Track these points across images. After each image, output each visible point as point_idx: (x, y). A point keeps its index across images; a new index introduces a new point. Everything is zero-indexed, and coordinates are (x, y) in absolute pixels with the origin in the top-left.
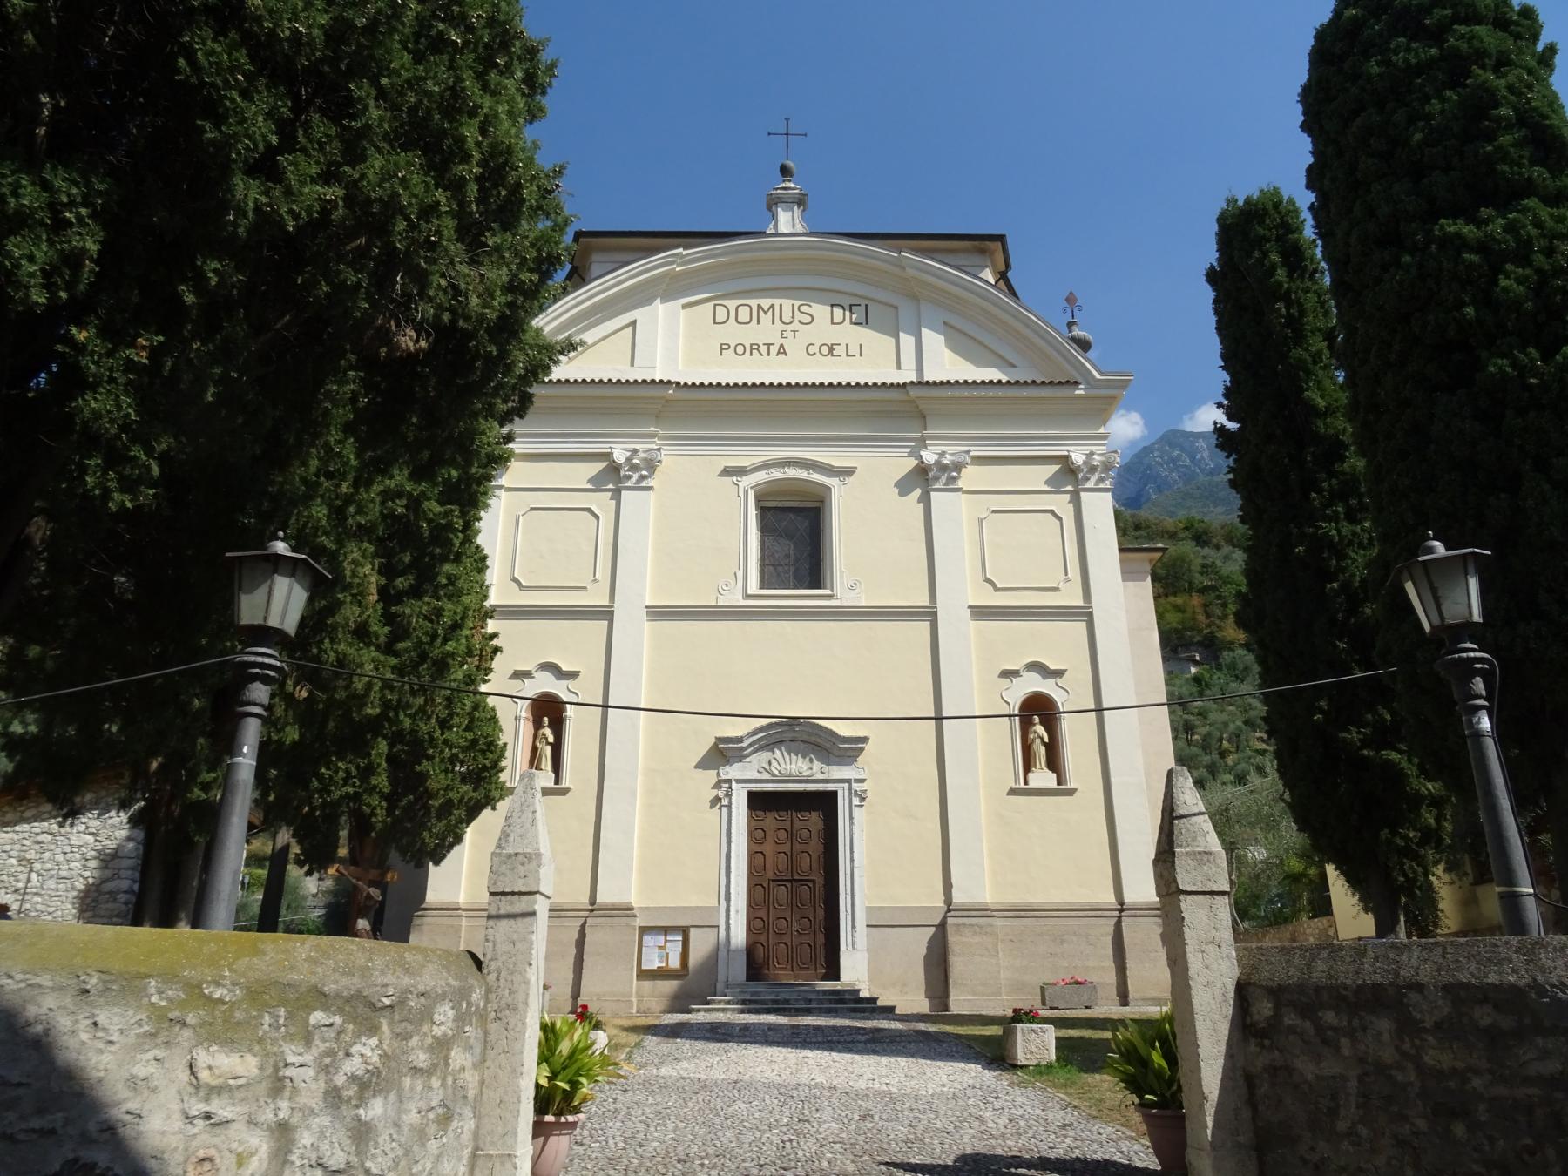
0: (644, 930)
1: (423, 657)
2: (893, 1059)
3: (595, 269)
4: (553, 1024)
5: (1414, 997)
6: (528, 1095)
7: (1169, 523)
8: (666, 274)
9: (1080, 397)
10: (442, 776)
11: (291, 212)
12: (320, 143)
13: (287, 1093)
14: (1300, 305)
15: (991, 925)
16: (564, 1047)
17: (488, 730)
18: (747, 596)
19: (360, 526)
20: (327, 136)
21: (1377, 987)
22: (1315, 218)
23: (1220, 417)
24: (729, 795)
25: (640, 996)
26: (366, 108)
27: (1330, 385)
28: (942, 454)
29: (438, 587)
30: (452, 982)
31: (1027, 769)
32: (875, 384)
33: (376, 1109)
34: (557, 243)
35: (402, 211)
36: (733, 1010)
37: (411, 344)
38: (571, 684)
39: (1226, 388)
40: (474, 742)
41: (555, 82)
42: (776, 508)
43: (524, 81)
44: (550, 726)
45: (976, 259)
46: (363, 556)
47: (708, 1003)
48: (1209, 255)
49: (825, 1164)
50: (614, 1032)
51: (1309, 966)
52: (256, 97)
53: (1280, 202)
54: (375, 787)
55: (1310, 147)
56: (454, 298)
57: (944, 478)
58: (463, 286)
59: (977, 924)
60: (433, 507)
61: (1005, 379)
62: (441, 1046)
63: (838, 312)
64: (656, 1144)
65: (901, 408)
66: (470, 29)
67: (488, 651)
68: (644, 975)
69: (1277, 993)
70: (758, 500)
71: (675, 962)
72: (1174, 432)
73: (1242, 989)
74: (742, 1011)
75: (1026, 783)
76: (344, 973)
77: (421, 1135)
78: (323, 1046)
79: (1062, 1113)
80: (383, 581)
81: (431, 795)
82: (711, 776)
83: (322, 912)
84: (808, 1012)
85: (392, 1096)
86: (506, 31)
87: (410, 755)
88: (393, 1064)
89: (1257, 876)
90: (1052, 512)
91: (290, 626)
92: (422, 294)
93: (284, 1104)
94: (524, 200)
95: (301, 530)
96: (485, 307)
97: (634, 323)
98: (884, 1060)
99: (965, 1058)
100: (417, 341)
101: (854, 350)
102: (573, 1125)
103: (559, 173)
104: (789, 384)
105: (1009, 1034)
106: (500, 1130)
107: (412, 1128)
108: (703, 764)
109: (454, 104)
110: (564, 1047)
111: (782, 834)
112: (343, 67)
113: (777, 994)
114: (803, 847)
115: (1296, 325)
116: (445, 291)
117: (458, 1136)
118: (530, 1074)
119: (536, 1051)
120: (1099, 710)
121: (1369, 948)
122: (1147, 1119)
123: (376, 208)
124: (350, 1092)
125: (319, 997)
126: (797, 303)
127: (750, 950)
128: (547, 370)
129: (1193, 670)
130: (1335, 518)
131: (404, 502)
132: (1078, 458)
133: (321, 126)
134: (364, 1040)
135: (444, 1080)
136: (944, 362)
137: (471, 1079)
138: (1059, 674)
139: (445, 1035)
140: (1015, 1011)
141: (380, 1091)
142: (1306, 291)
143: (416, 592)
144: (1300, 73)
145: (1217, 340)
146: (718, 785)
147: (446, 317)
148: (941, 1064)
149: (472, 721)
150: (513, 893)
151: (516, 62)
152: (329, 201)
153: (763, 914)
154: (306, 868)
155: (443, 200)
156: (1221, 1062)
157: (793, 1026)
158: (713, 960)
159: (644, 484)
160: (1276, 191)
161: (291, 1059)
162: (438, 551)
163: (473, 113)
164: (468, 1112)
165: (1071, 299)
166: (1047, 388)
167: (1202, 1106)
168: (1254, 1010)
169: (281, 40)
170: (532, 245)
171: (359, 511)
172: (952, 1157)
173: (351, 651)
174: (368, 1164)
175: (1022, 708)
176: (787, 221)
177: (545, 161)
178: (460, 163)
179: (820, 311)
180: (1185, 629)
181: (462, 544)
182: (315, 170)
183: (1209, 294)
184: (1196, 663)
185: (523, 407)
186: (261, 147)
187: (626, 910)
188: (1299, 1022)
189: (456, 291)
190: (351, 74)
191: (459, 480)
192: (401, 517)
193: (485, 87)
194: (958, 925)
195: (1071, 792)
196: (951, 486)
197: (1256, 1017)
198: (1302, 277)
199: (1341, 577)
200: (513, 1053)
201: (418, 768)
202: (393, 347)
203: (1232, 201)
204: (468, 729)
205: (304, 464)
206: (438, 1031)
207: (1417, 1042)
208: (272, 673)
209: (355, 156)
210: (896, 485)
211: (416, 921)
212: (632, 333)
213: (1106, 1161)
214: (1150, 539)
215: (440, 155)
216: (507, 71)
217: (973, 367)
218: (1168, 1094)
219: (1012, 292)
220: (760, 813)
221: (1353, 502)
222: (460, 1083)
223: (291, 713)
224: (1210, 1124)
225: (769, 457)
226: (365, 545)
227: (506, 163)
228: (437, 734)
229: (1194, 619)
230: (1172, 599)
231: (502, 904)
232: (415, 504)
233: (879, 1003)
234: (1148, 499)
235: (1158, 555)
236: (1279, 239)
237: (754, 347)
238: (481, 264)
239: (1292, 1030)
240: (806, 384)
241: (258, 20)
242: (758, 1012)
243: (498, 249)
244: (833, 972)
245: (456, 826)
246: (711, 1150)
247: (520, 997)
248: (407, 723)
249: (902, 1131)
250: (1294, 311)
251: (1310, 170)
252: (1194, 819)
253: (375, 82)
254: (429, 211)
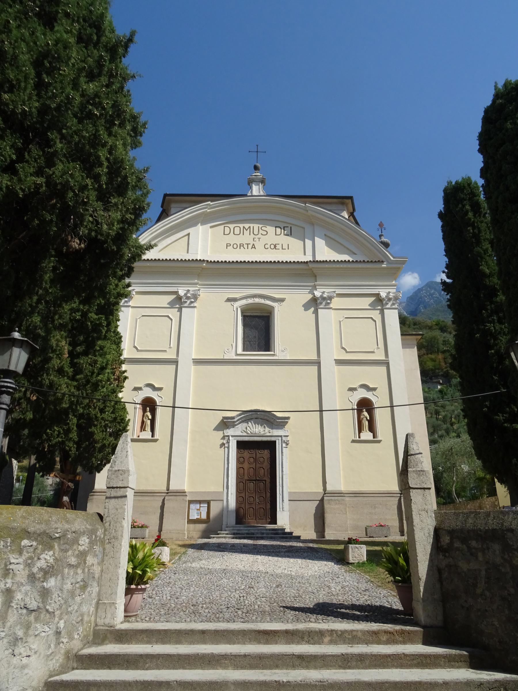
0: (190, 502)
1: (88, 382)
2: (295, 560)
3: (173, 210)
4: (136, 545)
5: (509, 534)
6: (123, 577)
7: (429, 322)
8: (203, 213)
9: (384, 268)
10: (101, 434)
11: (21, 189)
12: (35, 159)
13: (11, 576)
14: (479, 228)
15: (343, 500)
16: (140, 555)
17: (121, 413)
18: (237, 355)
19: (60, 324)
20: (38, 155)
21: (494, 530)
22: (484, 191)
23: (444, 277)
24: (228, 442)
25: (188, 531)
26: (55, 143)
27: (490, 265)
28: (323, 293)
29: (95, 351)
30: (88, 527)
31: (360, 431)
32: (294, 262)
33: (51, 583)
34: (143, 201)
35: (71, 189)
36: (229, 537)
37: (77, 246)
38: (159, 393)
39: (447, 264)
40: (115, 419)
41: (146, 130)
42: (251, 316)
43: (132, 130)
44: (150, 411)
45: (341, 207)
46: (61, 338)
47: (218, 534)
48: (440, 206)
49: (257, 607)
50: (174, 547)
51: (465, 521)
52: (6, 138)
53: (471, 183)
54: (71, 438)
55: (482, 160)
56: (96, 226)
57: (324, 303)
58: (100, 221)
59: (337, 500)
60: (93, 316)
61: (351, 260)
62: (83, 555)
63: (278, 230)
64: (184, 598)
65: (306, 272)
66: (104, 108)
67: (121, 379)
68: (190, 521)
69: (451, 533)
70: (242, 312)
71: (204, 516)
72: (433, 282)
73: (437, 530)
74: (233, 538)
75: (359, 437)
76: (38, 523)
77: (72, 594)
78: (27, 555)
79: (365, 584)
80: (71, 348)
81: (97, 442)
82: (220, 434)
83: (52, 493)
84: (262, 538)
85: (59, 577)
86: (119, 110)
87: (86, 423)
88: (60, 563)
89: (464, 478)
90: (372, 318)
91: (20, 369)
92: (82, 224)
93: (9, 581)
94: (128, 183)
95: (28, 327)
96: (110, 229)
97: (189, 234)
98: (292, 560)
99: (327, 560)
100: (80, 244)
101: (285, 246)
102: (144, 590)
103: (146, 171)
104: (256, 262)
105: (346, 549)
106: (110, 592)
107: (68, 591)
108: (218, 428)
109: (95, 141)
110: (140, 555)
111: (252, 460)
112: (45, 125)
113: (249, 530)
114: (260, 466)
115: (477, 237)
116: (92, 223)
117: (90, 595)
118: (124, 567)
119: (127, 557)
120: (321, 411)
121: (492, 513)
122: (398, 587)
123: (59, 187)
124: (40, 575)
125: (27, 534)
126: (260, 226)
127: (237, 511)
128: (140, 256)
129: (439, 387)
130: (493, 322)
131: (80, 313)
132: (383, 294)
133: (35, 150)
134: (46, 552)
135: (84, 570)
136: (325, 253)
137: (97, 570)
138: (374, 389)
139: (84, 550)
140: (349, 538)
141: (53, 575)
142: (482, 222)
143: (86, 353)
144: (478, 127)
145: (443, 243)
146: (223, 438)
147: (93, 234)
148: (316, 562)
149: (114, 410)
150: (117, 487)
151: (127, 123)
152: (39, 184)
153: (243, 495)
154: (41, 474)
155: (90, 183)
156: (427, 563)
157: (254, 545)
158: (220, 516)
159: (192, 305)
160: (469, 178)
161: (12, 561)
162: (95, 335)
163: (104, 145)
164: (95, 584)
165: (381, 225)
166: (370, 264)
167: (418, 582)
168: (442, 540)
169: (17, 114)
170: (132, 202)
171: (60, 317)
172: (313, 604)
173: (55, 379)
174: (48, 607)
175: (357, 405)
176: (256, 190)
177: (139, 165)
178: (98, 167)
179: (271, 229)
180: (436, 369)
181: (106, 332)
182: (32, 170)
183: (440, 223)
184: (441, 384)
185: (129, 272)
186: (8, 160)
187: (183, 493)
188: (461, 545)
189: (97, 223)
190: (50, 128)
191: (105, 304)
192: (78, 321)
193: (110, 134)
194: (329, 500)
195: (379, 442)
196: (327, 306)
197: (443, 543)
198: (480, 216)
199: (495, 348)
200: (116, 558)
201: (90, 430)
202: (69, 247)
203: (450, 183)
204: (113, 412)
205: (31, 298)
206: (81, 548)
207: (510, 554)
208: (11, 390)
209: (50, 163)
210: (303, 306)
211: (90, 497)
212: (163, 242)
213: (381, 606)
214: (421, 329)
215: (89, 164)
216: (122, 125)
217: (337, 255)
218: (406, 577)
219: (357, 223)
220: (242, 450)
221: (501, 315)
222: (91, 571)
223: (29, 406)
224: (422, 590)
225: (248, 294)
226: (62, 333)
227: (120, 167)
228: (99, 415)
229: (440, 365)
230: (430, 356)
231: (112, 492)
232: (84, 315)
233: (294, 535)
234: (420, 311)
235: (420, 337)
236: (470, 199)
237: (242, 245)
238: (109, 210)
239: (458, 549)
240: (264, 262)
241: (7, 105)
242: (240, 538)
243: (116, 204)
244: (274, 521)
245: (107, 456)
246: (207, 601)
247: (119, 533)
248: (81, 411)
249: (292, 592)
250: (476, 231)
251: (482, 170)
252: (417, 456)
253: (60, 132)
254: (83, 188)
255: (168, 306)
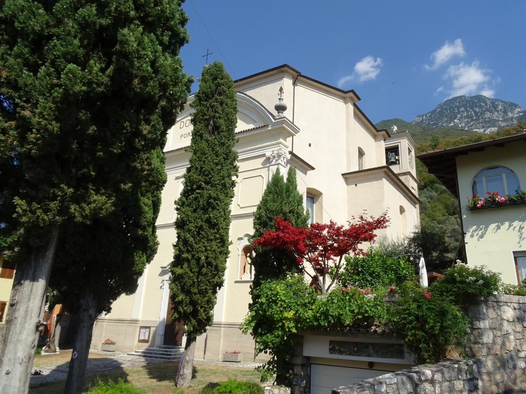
9: (269, 130)
255: (262, 166)
